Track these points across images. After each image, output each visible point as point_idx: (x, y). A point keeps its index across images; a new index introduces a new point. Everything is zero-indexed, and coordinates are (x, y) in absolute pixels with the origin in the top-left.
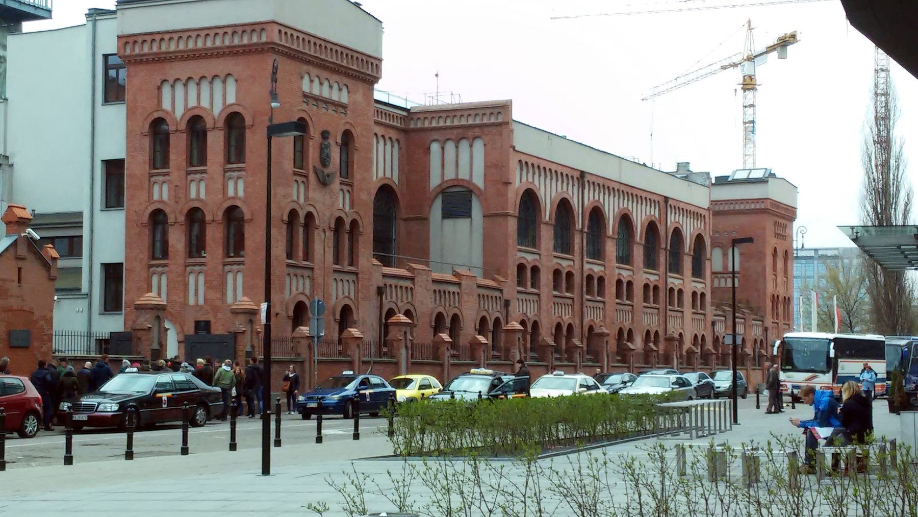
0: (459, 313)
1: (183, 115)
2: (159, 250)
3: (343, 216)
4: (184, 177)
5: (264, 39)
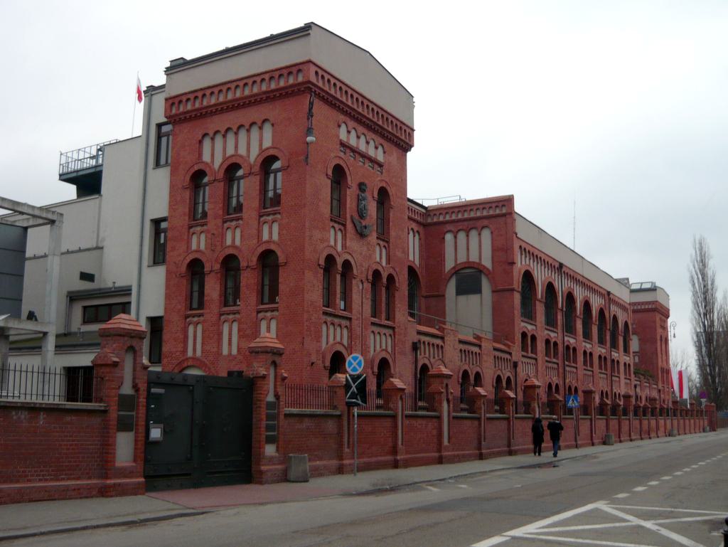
0: (480, 371)
1: (222, 164)
2: (196, 301)
3: (380, 269)
4: (220, 224)
5: (300, 79)
